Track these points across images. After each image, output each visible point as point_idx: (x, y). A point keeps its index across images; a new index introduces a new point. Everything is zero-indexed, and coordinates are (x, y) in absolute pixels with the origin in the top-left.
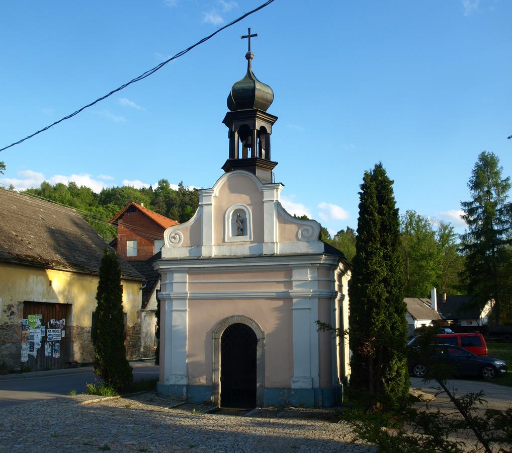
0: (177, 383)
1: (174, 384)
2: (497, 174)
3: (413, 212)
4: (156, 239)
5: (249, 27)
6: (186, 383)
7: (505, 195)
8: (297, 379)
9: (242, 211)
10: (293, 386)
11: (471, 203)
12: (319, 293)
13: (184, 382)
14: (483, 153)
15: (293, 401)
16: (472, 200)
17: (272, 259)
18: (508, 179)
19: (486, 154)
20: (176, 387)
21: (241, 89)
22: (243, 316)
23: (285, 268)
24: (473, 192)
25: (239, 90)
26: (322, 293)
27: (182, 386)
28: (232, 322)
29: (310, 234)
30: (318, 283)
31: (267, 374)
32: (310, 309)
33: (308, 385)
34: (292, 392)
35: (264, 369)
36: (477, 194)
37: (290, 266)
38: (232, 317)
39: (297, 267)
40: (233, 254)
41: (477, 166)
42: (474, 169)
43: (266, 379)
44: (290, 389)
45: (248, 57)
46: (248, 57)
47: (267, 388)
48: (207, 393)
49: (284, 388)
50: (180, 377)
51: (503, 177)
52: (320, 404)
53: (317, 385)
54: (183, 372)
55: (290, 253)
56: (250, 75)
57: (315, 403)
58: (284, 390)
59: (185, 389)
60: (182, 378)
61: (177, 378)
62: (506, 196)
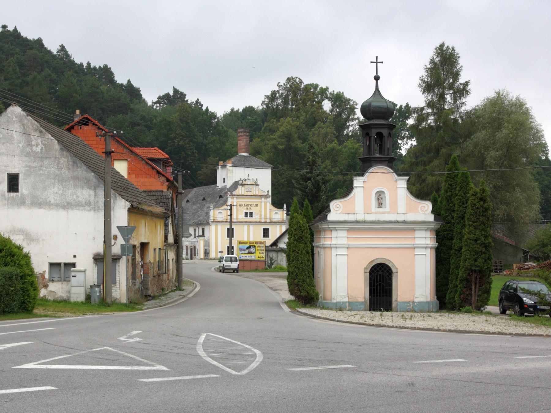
0: (342, 301)
2: (456, 75)
3: (297, 80)
4: (116, 160)
6: (347, 300)
9: (383, 192)
10: (416, 300)
11: (422, 109)
13: (346, 300)
14: (442, 46)
17: (405, 224)
18: (466, 84)
19: (445, 48)
21: (377, 107)
22: (384, 259)
25: (376, 107)
27: (346, 302)
28: (390, 265)
29: (426, 209)
31: (399, 294)
32: (425, 254)
34: (416, 304)
35: (397, 291)
36: (430, 97)
40: (377, 220)
41: (432, 61)
42: (429, 66)
44: (413, 302)
45: (377, 78)
46: (377, 78)
47: (399, 302)
50: (343, 297)
51: (462, 80)
53: (429, 300)
54: (345, 294)
59: (347, 304)
60: (345, 297)
61: (342, 297)
62: (464, 103)
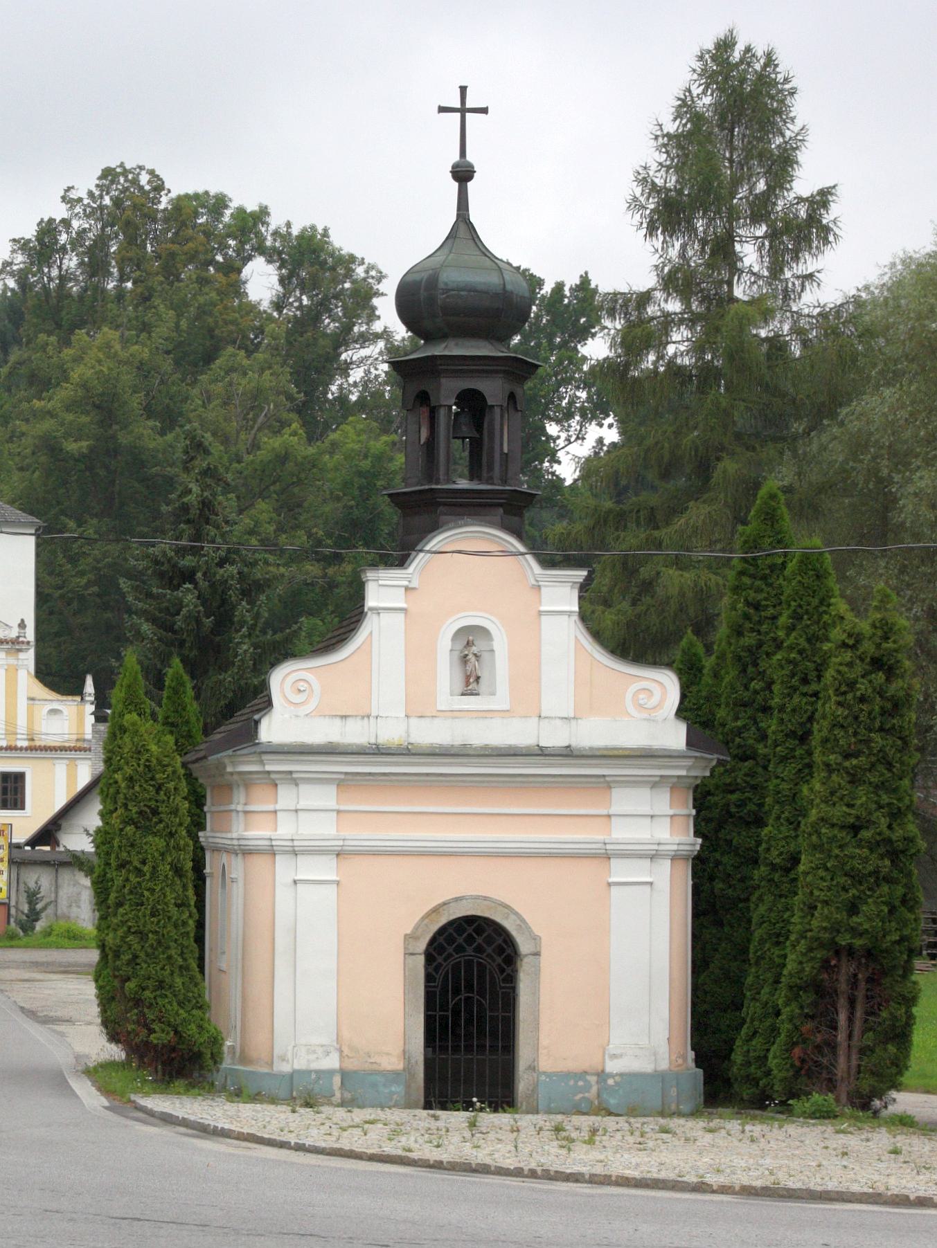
1: (304, 1068)
3: (144, 179)
5: (463, 84)
7: (801, 269)
8: (618, 1052)
9: (482, 632)
10: (612, 1067)
11: (645, 298)
12: (675, 847)
14: (725, 45)
15: (612, 1101)
16: (645, 280)
18: (822, 199)
19: (736, 55)
20: (313, 1076)
22: (485, 898)
23: (594, 783)
24: (658, 242)
26: (682, 847)
27: (331, 1072)
29: (654, 701)
30: (672, 823)
31: (544, 1041)
32: (651, 884)
33: (648, 1067)
34: (611, 1082)
36: (674, 252)
37: (607, 779)
38: (457, 900)
39: (635, 782)
41: (685, 107)
42: (671, 127)
43: (541, 1051)
44: (602, 1075)
45: (463, 174)
46: (463, 174)
47: (544, 1073)
48: (393, 1089)
49: (586, 1072)
50: (320, 1050)
52: (673, 1107)
55: (607, 749)
56: (463, 228)
57: (663, 1104)
58: (588, 1078)
59: (337, 1080)
60: (328, 1053)
61: (314, 1052)
62: (810, 276)
